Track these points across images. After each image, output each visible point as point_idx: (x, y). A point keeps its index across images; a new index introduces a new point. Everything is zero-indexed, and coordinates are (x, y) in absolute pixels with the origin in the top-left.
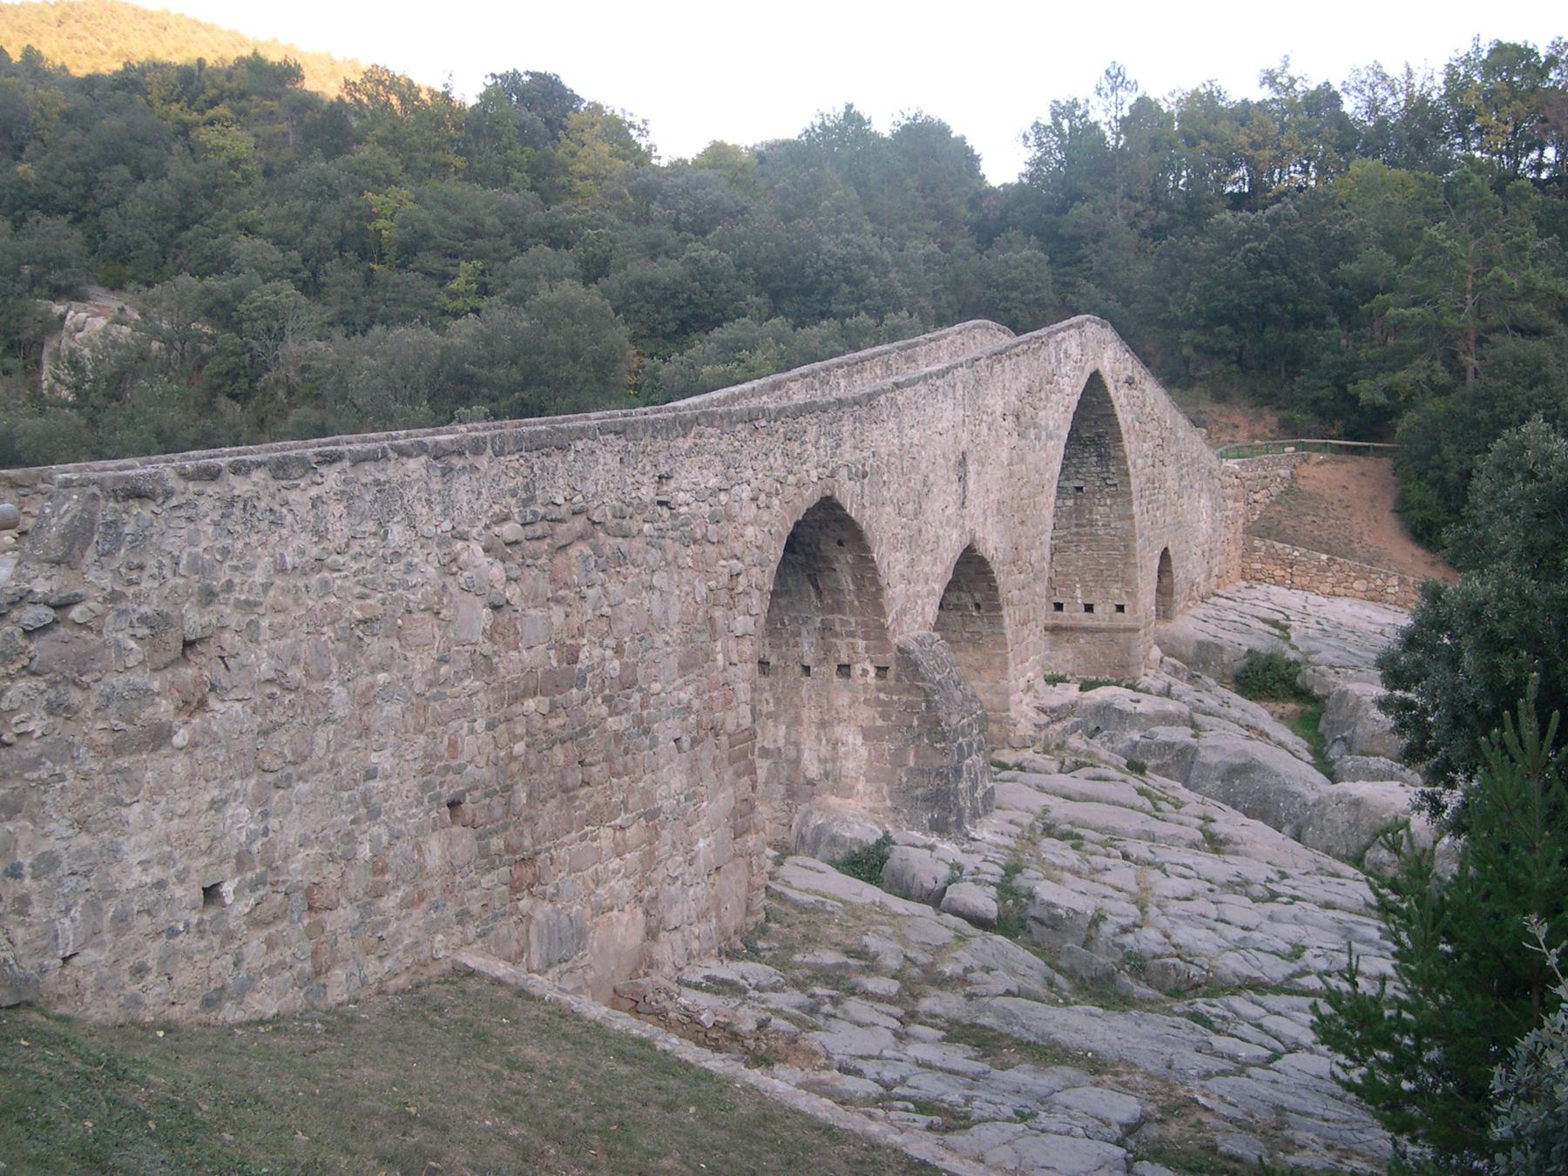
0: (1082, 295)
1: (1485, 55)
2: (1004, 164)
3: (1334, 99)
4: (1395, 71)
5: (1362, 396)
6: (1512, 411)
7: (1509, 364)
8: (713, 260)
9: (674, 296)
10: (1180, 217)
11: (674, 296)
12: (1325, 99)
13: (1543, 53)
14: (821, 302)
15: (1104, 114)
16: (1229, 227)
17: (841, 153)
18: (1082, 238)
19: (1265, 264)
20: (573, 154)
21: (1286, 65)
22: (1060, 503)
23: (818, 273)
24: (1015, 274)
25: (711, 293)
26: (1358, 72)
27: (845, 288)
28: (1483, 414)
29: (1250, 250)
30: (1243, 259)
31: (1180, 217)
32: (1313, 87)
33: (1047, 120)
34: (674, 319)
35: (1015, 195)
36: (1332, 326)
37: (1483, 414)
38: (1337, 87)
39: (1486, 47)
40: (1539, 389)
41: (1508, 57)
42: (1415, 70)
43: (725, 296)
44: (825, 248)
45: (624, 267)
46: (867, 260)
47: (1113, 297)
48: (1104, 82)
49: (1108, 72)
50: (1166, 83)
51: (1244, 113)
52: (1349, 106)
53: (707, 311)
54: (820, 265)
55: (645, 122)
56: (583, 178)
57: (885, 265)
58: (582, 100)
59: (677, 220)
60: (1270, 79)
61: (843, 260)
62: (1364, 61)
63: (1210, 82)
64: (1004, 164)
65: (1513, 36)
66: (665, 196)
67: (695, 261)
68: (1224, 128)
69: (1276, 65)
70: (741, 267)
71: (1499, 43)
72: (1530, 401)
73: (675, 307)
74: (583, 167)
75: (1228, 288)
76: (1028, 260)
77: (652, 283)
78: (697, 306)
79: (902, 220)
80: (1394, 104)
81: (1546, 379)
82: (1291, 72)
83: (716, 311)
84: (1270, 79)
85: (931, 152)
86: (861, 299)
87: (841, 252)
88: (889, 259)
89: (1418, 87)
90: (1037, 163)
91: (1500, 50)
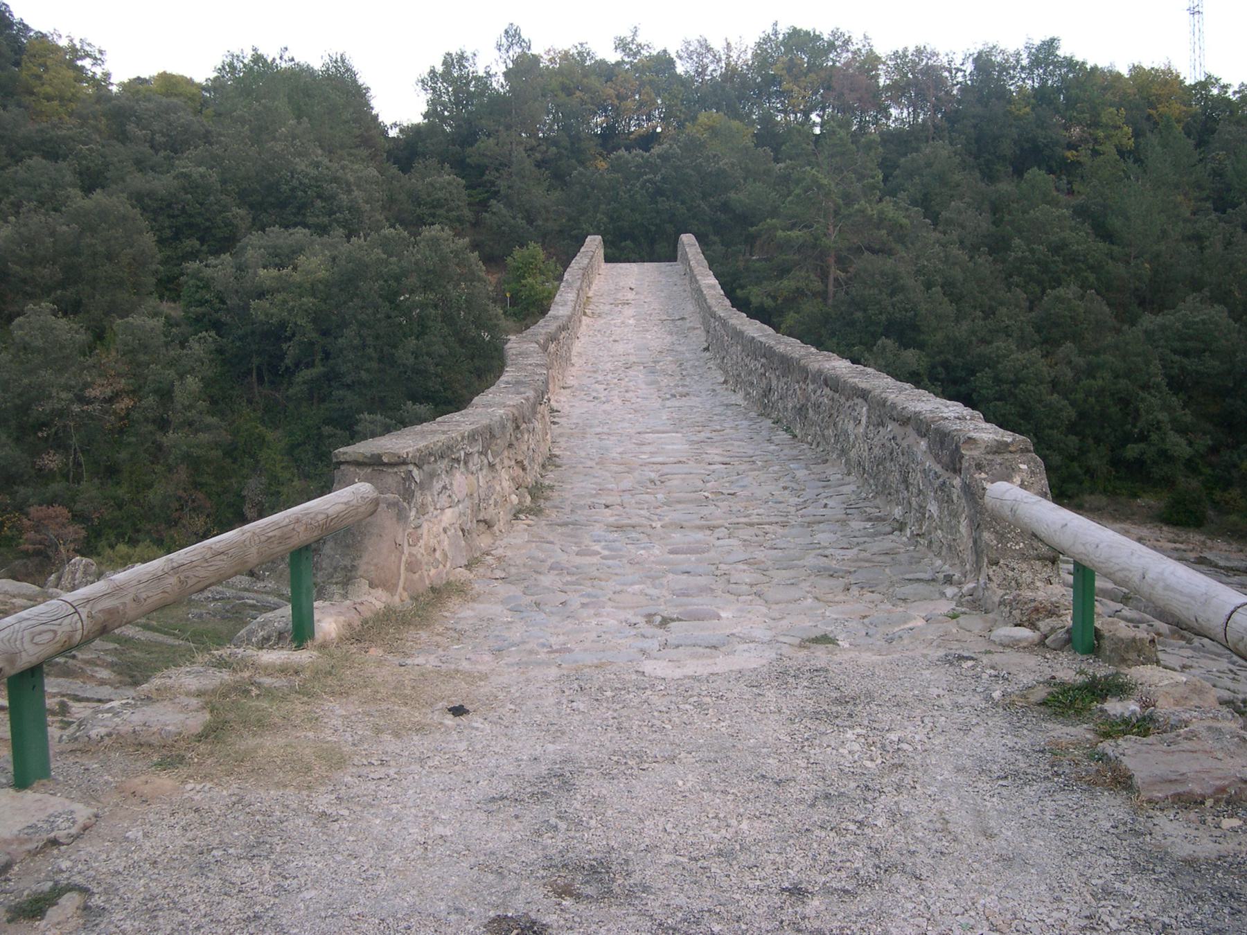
0: (494, 213)
1: (781, 37)
2: (399, 105)
3: (671, 63)
4: (718, 45)
5: (753, 299)
6: (881, 313)
7: (877, 277)
8: (202, 176)
9: (169, 206)
10: (565, 153)
11: (169, 206)
12: (663, 62)
13: (826, 37)
14: (294, 215)
15: (491, 63)
16: (627, 162)
17: (260, 90)
18: (487, 168)
19: (659, 192)
20: (39, 77)
21: (635, 34)
22: (1017, 480)
23: (293, 190)
24: (440, 194)
25: (201, 204)
26: (689, 43)
27: (319, 203)
28: (859, 315)
29: (648, 181)
30: (642, 188)
31: (565, 153)
32: (655, 53)
33: (440, 69)
34: (170, 227)
35: (413, 134)
36: (714, 243)
37: (859, 315)
38: (673, 55)
39: (783, 29)
40: (900, 297)
41: (799, 40)
42: (733, 45)
43: (216, 207)
44: (299, 168)
45: (123, 180)
46: (335, 180)
47: (520, 215)
48: (504, 40)
49: (506, 32)
50: (549, 40)
51: (607, 72)
52: (680, 68)
53: (199, 220)
54: (295, 183)
55: (101, 52)
56: (49, 98)
57: (348, 184)
58: (31, 30)
59: (153, 139)
60: (622, 45)
61: (316, 179)
62: (693, 37)
63: (581, 45)
64: (399, 105)
65: (805, 25)
66: (139, 119)
67: (186, 176)
68: (594, 82)
69: (628, 35)
70: (224, 182)
71: (795, 29)
72: (893, 305)
73: (169, 216)
74: (48, 89)
75: (632, 210)
76: (449, 183)
77: (151, 194)
78: (191, 216)
79: (342, 147)
80: (715, 70)
81: (903, 289)
82: (639, 40)
83: (208, 220)
84: (622, 45)
85: (332, 97)
86: (331, 213)
87: (313, 172)
88: (352, 180)
89: (735, 57)
90: (433, 103)
91: (795, 33)
